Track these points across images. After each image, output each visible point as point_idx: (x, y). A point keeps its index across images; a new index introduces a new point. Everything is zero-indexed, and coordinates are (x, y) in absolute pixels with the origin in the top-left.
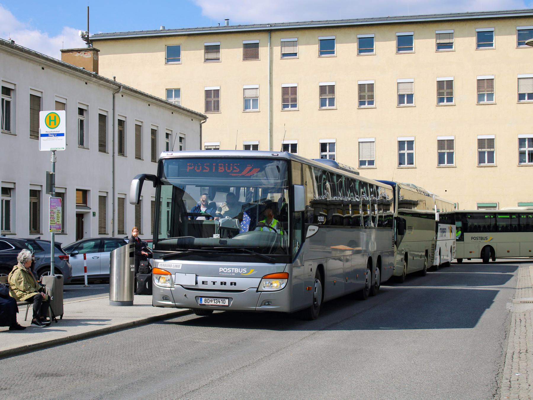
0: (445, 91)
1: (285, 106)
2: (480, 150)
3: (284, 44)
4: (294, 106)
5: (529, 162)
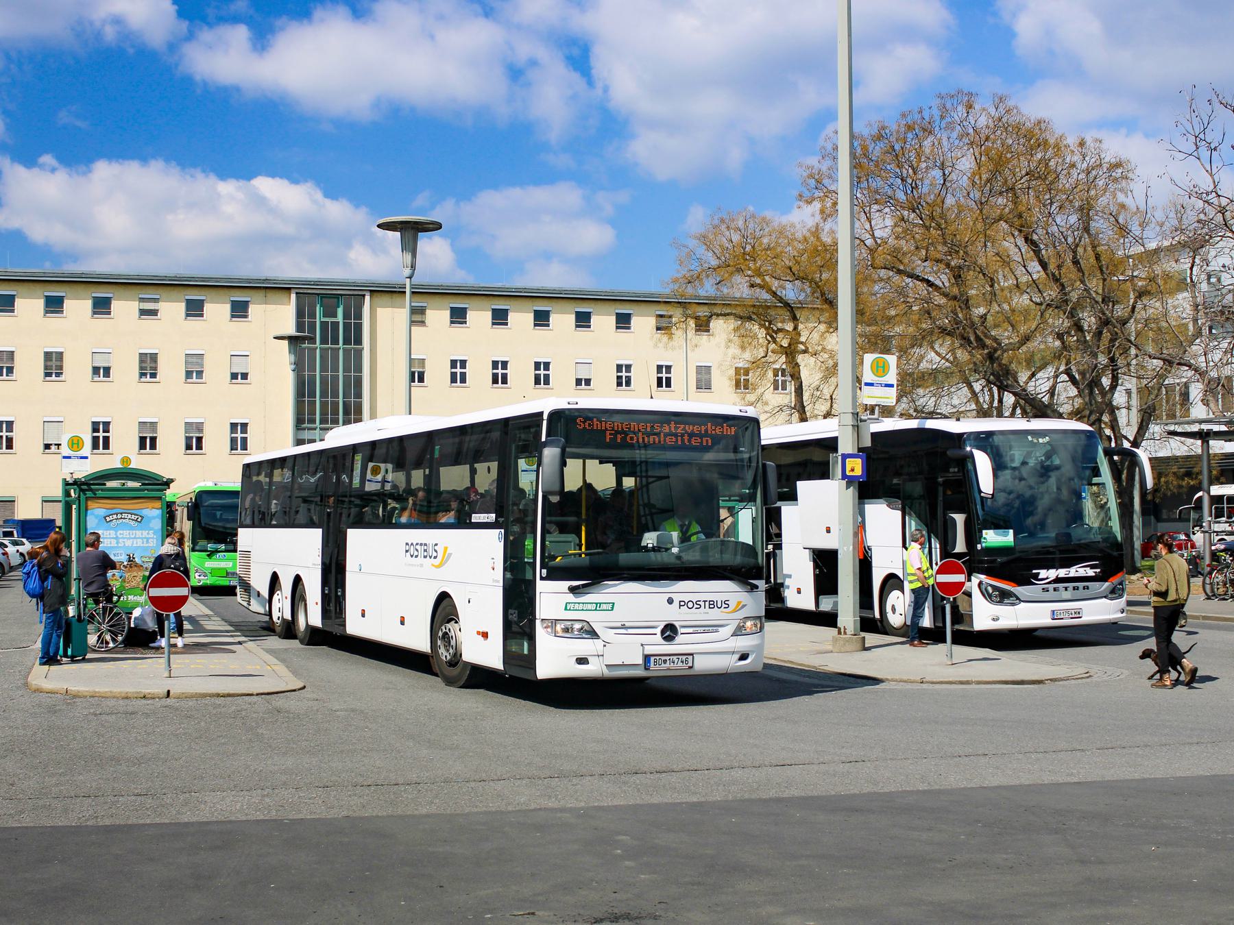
0: (148, 364)
2: (187, 435)
3: (142, 300)
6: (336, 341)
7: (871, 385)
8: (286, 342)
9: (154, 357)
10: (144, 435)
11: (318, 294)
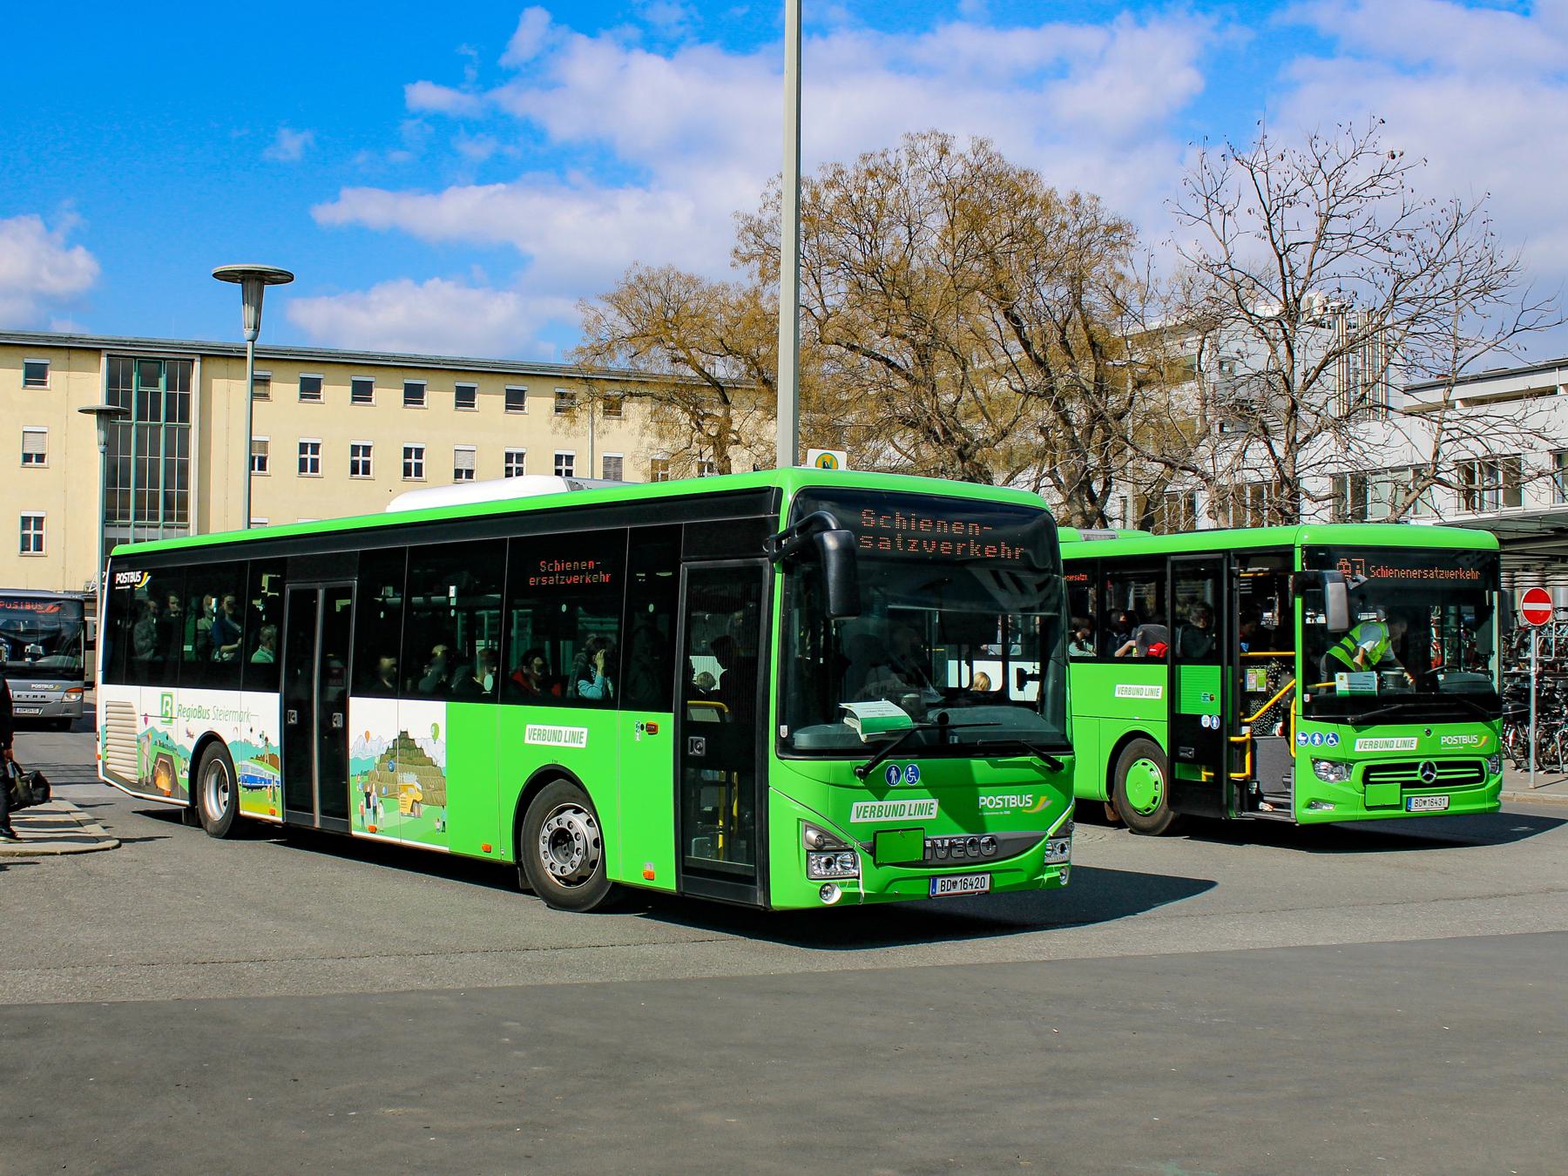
6: (156, 417)
11: (135, 358)
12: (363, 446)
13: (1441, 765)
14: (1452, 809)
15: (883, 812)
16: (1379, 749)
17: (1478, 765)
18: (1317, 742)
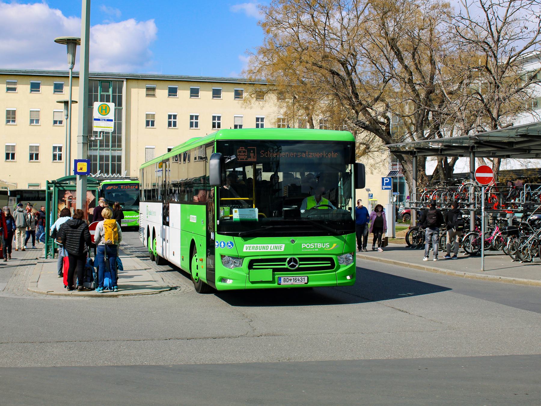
0: (11, 116)
1: (8, 121)
3: (8, 83)
4: (14, 121)
5: (59, 160)
7: (99, 120)
8: (63, 104)
9: (14, 112)
10: (8, 152)
11: (99, 80)
12: (195, 116)
13: (301, 259)
14: (311, 284)
15: (258, 248)
16: (258, 250)
17: (331, 260)
18: (222, 246)
